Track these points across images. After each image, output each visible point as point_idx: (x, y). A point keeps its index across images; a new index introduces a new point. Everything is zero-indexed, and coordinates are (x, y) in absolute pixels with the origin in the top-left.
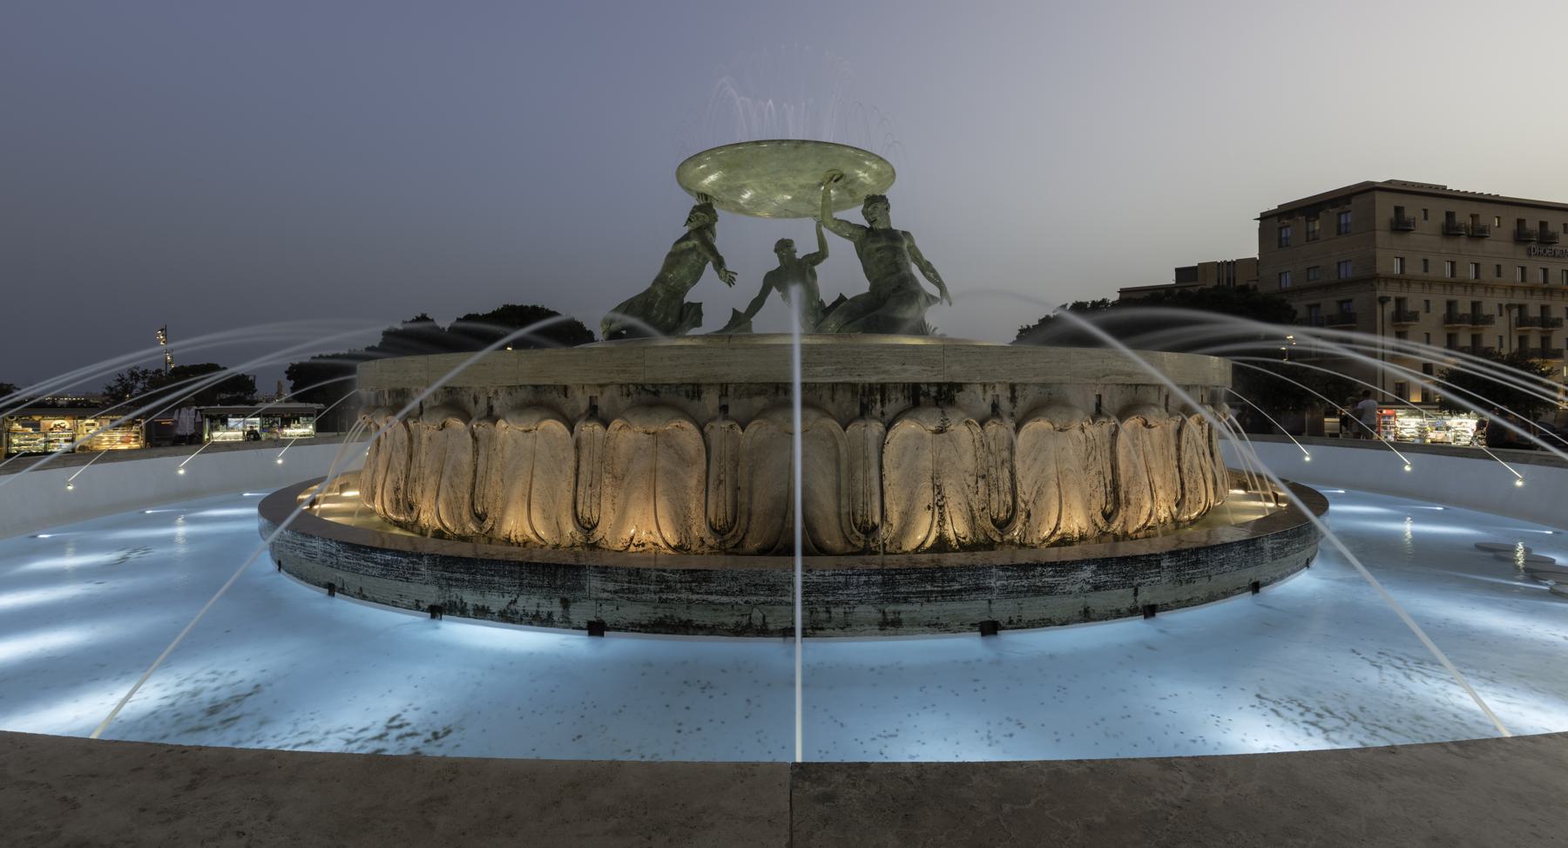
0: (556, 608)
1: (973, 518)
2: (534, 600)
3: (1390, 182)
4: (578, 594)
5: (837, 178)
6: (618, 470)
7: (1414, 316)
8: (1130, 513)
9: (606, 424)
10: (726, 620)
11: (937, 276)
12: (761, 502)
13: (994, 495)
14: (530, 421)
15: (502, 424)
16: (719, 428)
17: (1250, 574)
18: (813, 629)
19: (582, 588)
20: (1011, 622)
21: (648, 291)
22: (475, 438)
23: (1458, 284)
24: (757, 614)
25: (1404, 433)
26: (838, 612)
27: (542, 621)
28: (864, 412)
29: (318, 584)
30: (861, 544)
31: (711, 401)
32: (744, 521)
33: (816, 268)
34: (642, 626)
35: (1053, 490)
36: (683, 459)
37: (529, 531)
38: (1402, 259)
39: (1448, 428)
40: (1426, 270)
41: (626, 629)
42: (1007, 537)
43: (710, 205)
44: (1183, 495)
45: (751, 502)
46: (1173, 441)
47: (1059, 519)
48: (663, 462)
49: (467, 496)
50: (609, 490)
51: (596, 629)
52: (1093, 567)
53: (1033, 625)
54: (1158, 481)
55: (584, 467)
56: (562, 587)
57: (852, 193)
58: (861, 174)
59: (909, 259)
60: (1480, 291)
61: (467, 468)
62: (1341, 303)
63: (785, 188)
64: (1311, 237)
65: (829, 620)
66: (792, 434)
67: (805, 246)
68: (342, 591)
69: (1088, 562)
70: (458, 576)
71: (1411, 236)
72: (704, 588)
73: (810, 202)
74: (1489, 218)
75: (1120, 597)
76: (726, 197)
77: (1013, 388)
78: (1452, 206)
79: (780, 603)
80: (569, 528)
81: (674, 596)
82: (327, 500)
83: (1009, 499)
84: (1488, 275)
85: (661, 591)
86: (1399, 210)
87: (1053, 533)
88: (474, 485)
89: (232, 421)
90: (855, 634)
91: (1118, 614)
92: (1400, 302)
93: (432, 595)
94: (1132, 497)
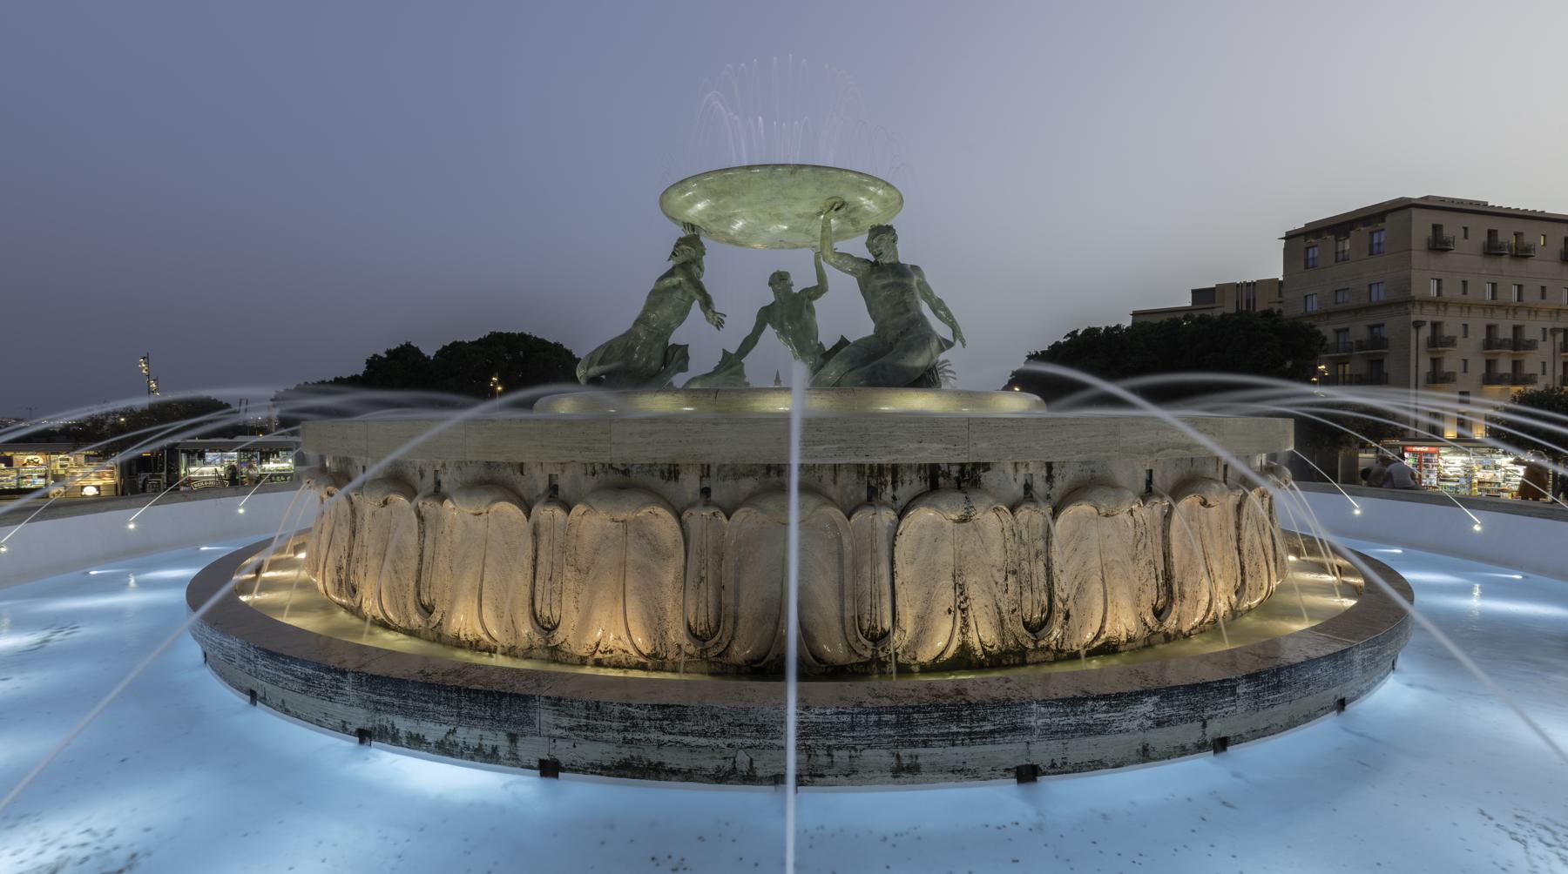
0: (502, 742)
1: (1002, 621)
2: (477, 732)
3: (1426, 198)
4: (527, 729)
5: (839, 206)
6: (582, 562)
7: (1451, 342)
8: (1185, 608)
9: (568, 509)
10: (705, 764)
11: (949, 314)
12: (749, 603)
13: (1027, 594)
14: (480, 503)
15: (448, 504)
16: (699, 517)
17: (1336, 692)
18: (809, 776)
19: (531, 723)
20: (1053, 766)
21: (629, 332)
22: (421, 517)
23: (1499, 306)
24: (742, 758)
25: (1447, 472)
26: (841, 756)
27: (484, 756)
28: (873, 497)
29: (240, 689)
30: (868, 654)
31: (690, 484)
32: (729, 625)
33: (815, 303)
34: (603, 768)
35: (1096, 588)
36: (656, 550)
37: (480, 631)
38: (1439, 281)
39: (1497, 467)
40: (1465, 292)
41: (585, 771)
42: (1042, 643)
43: (697, 237)
44: (1243, 581)
45: (737, 603)
46: (1232, 519)
47: (1104, 621)
48: (633, 555)
49: (412, 584)
50: (571, 586)
51: (549, 769)
52: (1156, 699)
53: (1079, 768)
54: (1216, 566)
55: (543, 558)
56: (507, 719)
57: (855, 222)
58: (863, 200)
59: (918, 296)
60: (1522, 315)
61: (413, 552)
62: (1371, 327)
63: (779, 218)
64: (1340, 258)
65: (832, 764)
66: (786, 524)
67: (802, 279)
68: (264, 700)
69: (1149, 693)
70: (387, 699)
71: (1449, 255)
72: (678, 726)
73: (807, 232)
74: (1534, 236)
75: (1189, 733)
76: (714, 227)
77: (1049, 466)
78: (1494, 223)
79: (771, 747)
80: (526, 628)
81: (641, 736)
82: (274, 566)
83: (1045, 598)
84: (1531, 297)
85: (626, 729)
86: (1437, 228)
87: (1097, 637)
88: (419, 572)
89: (210, 456)
90: (863, 782)
91: (1183, 751)
92: (1436, 326)
93: (361, 718)
94: (1187, 589)
